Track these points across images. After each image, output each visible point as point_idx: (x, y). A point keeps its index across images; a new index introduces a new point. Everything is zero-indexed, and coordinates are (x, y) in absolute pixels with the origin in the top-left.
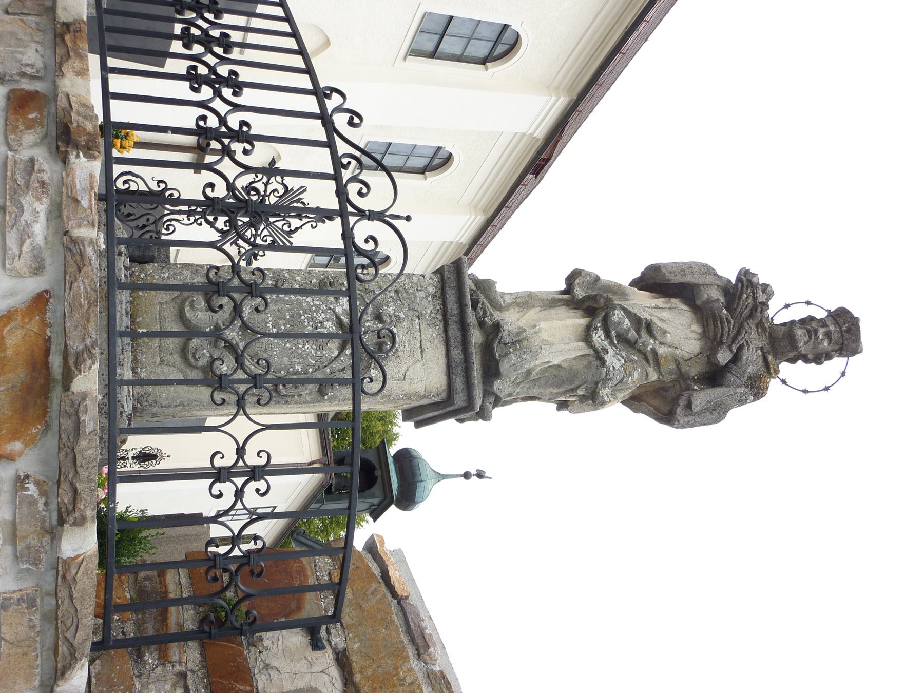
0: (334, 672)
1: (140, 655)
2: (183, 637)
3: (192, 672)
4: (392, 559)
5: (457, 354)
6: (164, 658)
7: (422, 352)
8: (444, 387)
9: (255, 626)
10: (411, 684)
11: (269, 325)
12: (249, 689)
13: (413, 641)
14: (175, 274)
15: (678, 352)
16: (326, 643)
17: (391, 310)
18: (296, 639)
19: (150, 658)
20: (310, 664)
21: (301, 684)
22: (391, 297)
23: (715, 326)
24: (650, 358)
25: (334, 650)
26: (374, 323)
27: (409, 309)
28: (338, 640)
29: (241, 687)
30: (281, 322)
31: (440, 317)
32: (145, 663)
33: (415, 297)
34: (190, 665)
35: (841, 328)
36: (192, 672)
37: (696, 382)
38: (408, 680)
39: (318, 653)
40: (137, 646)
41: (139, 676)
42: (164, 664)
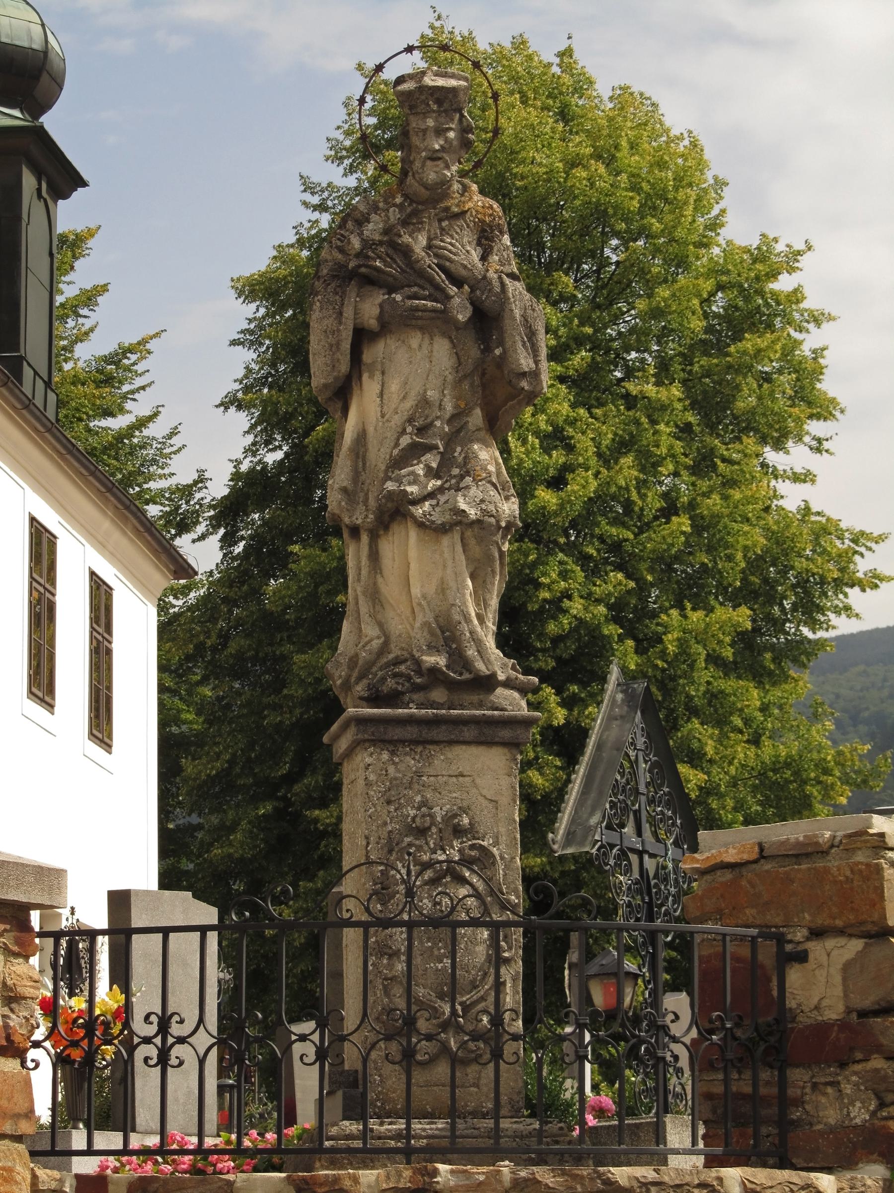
0: (830, 943)
1: (792, 1122)
2: (783, 1083)
3: (813, 1077)
4: (714, 851)
5: (469, 733)
6: (799, 1102)
7: (463, 776)
8: (506, 750)
9: (783, 1015)
10: (852, 871)
11: (440, 966)
12: (836, 1028)
13: (808, 855)
14: (376, 1069)
15: (450, 378)
16: (800, 948)
17: (412, 812)
18: (794, 976)
19: (796, 1114)
20: (821, 966)
21: (838, 979)
22: (396, 810)
23: (418, 318)
24: (457, 424)
25: (808, 939)
26: (431, 836)
27: (410, 788)
28: (800, 935)
29: (834, 1034)
30: (436, 952)
31: (419, 749)
32: (799, 1120)
33: (396, 779)
34: (806, 1078)
35: (434, 111)
36: (813, 1077)
37: (487, 350)
38: (848, 873)
39: (811, 956)
40: (785, 1125)
41: (811, 1124)
42: (803, 1102)
